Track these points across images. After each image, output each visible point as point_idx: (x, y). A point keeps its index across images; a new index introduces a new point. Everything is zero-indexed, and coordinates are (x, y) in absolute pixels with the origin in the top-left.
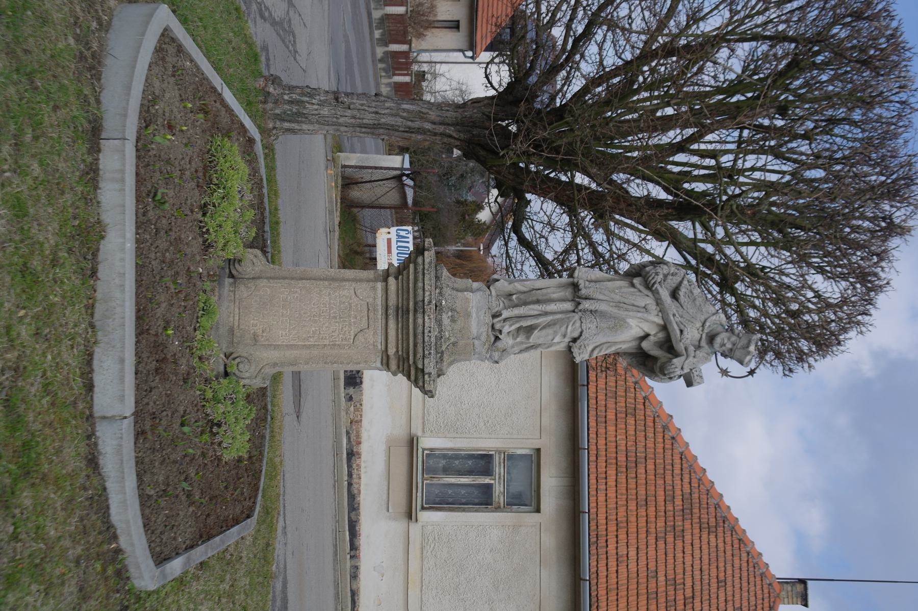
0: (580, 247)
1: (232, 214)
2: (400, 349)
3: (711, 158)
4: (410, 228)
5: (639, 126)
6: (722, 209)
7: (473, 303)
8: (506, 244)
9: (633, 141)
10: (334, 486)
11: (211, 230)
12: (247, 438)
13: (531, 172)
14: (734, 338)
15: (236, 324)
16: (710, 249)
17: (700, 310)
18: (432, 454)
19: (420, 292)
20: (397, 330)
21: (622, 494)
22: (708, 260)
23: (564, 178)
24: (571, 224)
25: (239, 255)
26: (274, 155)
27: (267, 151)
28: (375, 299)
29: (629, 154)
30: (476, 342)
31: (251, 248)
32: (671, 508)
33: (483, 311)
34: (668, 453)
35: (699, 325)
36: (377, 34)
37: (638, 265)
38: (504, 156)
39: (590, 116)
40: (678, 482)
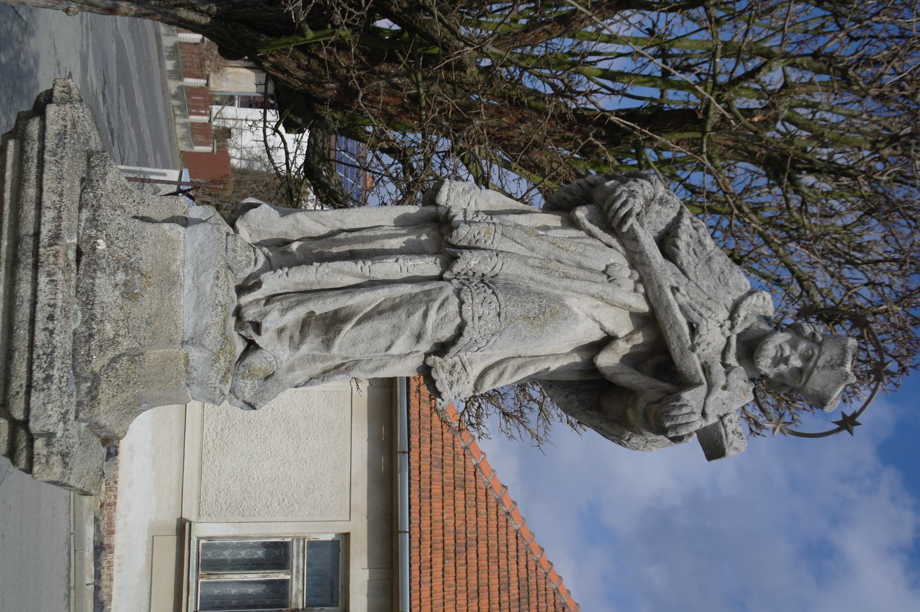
10: (69, 597)
18: (210, 544)
19: (29, 211)
30: (195, 354)
32: (506, 599)
33: (212, 274)
34: (503, 531)
35: (723, 315)
36: (169, 65)
40: (513, 566)
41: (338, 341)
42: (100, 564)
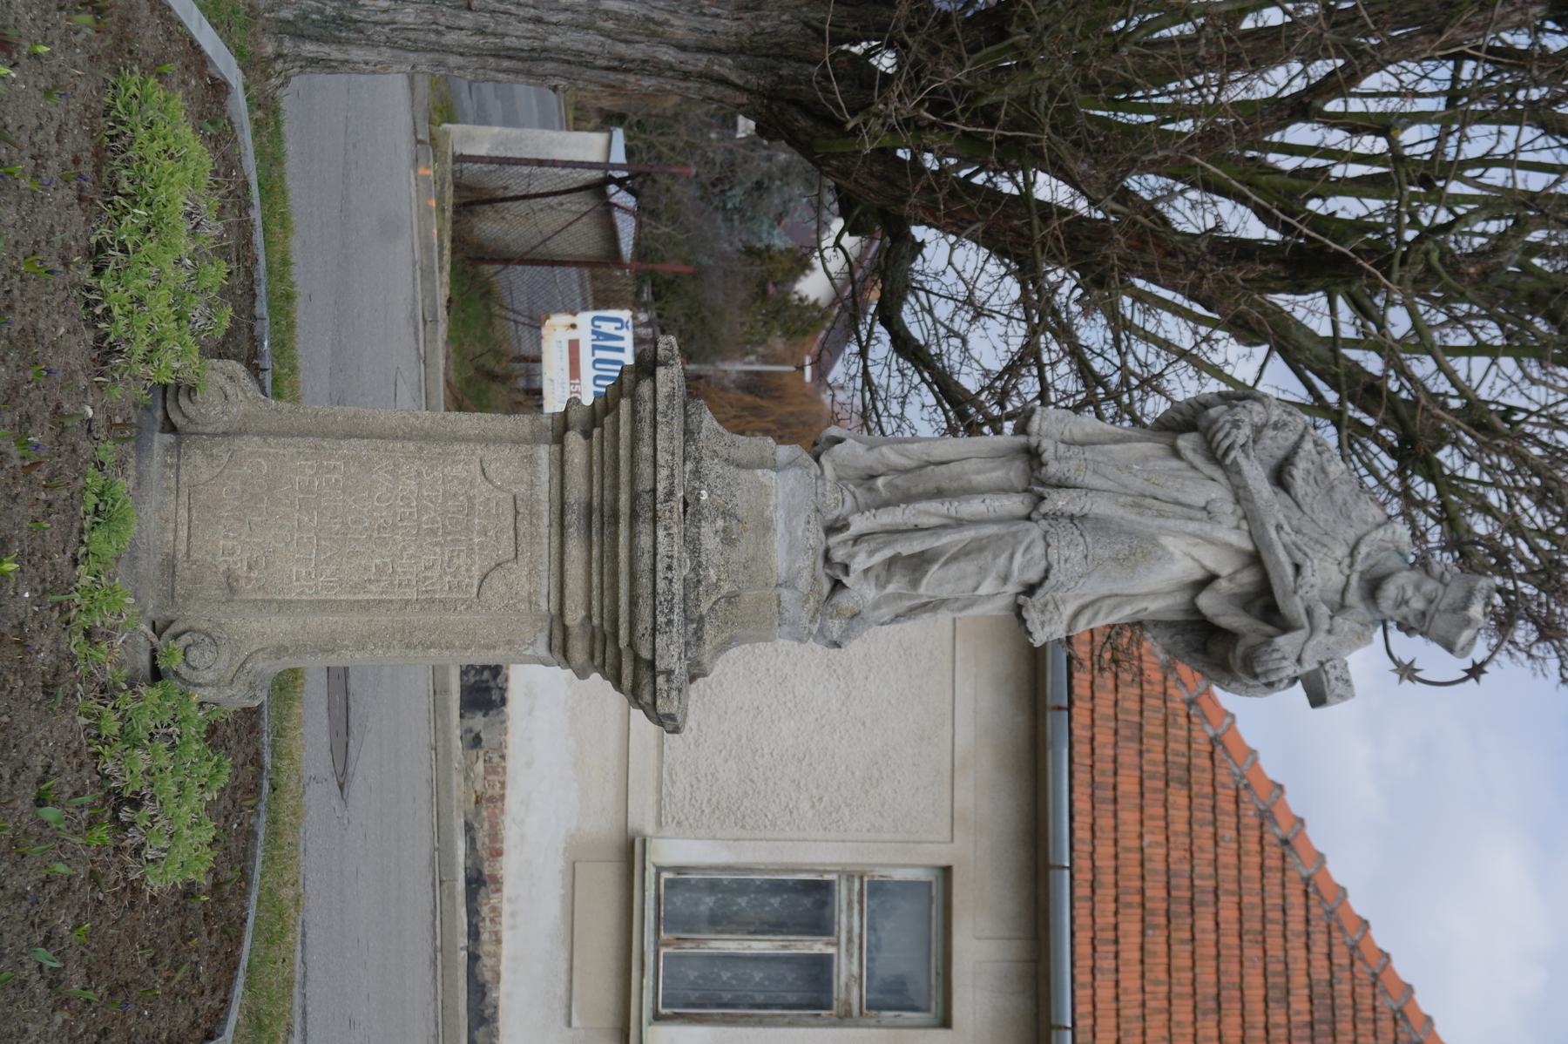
0: (1045, 359)
1: (169, 270)
2: (595, 610)
3: (1377, 133)
4: (625, 315)
5: (1194, 56)
6: (1403, 262)
7: (779, 494)
8: (863, 353)
9: (1178, 91)
11: (116, 311)
12: (208, 836)
13: (923, 170)
14: (1430, 586)
15: (183, 548)
16: (1373, 363)
17: (1345, 516)
18: (679, 880)
19: (645, 469)
20: (589, 563)
21: (1157, 983)
22: (1369, 392)
23: (1007, 187)
24: (1024, 301)
25: (188, 376)
26: (278, 124)
27: (259, 114)
28: (532, 485)
29: (1170, 127)
30: (786, 594)
31: (220, 357)
32: (1282, 1020)
33: (803, 518)
34: (1274, 879)
35: (1341, 551)
37: (1188, 402)
38: (855, 131)
39: (1071, 30)
40: (1297, 953)
41: (925, 582)
42: (478, 912)
